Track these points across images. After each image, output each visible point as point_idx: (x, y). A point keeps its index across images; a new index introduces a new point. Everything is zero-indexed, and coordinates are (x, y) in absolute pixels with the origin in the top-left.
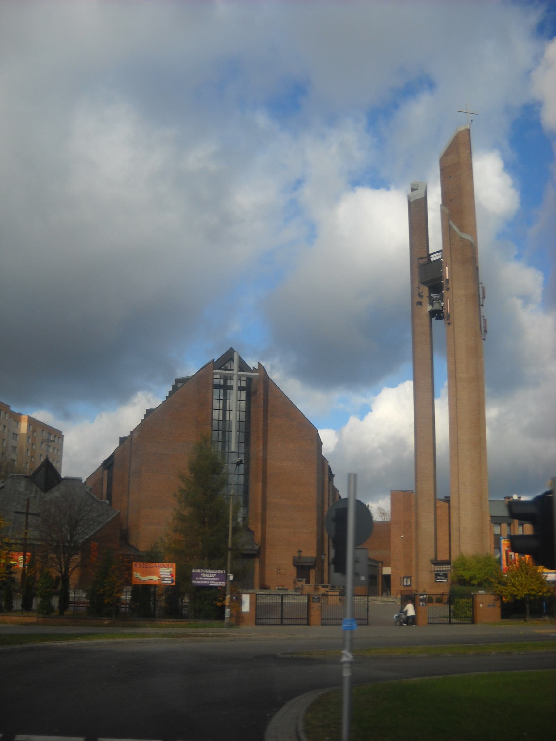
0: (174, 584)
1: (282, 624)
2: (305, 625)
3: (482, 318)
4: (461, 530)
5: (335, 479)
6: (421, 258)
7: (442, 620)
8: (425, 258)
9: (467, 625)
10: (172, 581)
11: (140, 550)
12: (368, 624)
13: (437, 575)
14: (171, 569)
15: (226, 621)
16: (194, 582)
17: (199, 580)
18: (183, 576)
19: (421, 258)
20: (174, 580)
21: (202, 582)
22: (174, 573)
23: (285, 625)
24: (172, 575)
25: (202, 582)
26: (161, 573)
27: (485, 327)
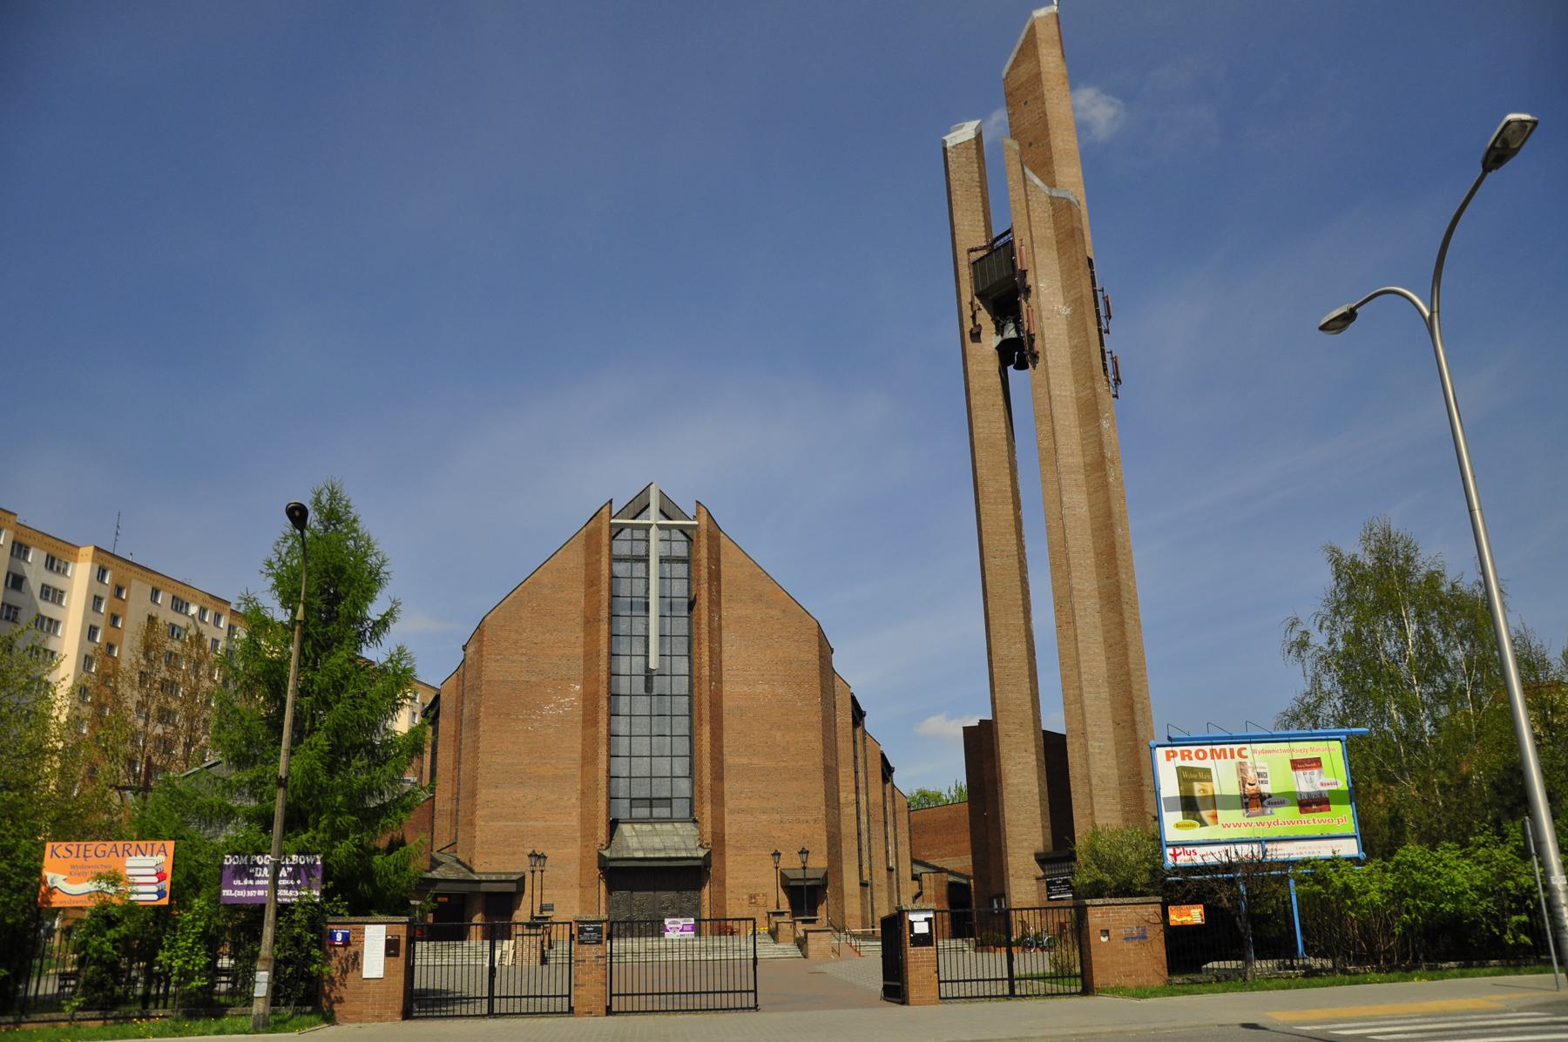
0: (165, 901)
1: (491, 1014)
2: (483, 1016)
3: (1108, 356)
4: (1095, 781)
5: (868, 722)
6: (975, 250)
7: (987, 988)
8: (982, 248)
9: (1064, 1001)
10: (161, 894)
11: (476, 869)
12: (756, 1008)
13: (1049, 884)
14: (161, 858)
15: (259, 1007)
16: (226, 893)
17: (240, 888)
18: (188, 881)
19: (975, 250)
20: (168, 890)
21: (251, 893)
22: (168, 871)
23: (501, 1015)
24: (161, 876)
25: (251, 893)
26: (129, 872)
27: (1116, 372)
